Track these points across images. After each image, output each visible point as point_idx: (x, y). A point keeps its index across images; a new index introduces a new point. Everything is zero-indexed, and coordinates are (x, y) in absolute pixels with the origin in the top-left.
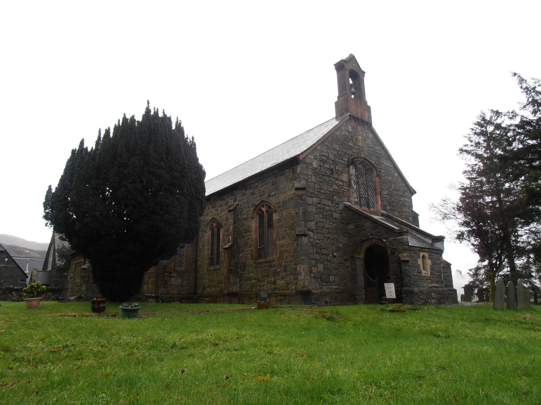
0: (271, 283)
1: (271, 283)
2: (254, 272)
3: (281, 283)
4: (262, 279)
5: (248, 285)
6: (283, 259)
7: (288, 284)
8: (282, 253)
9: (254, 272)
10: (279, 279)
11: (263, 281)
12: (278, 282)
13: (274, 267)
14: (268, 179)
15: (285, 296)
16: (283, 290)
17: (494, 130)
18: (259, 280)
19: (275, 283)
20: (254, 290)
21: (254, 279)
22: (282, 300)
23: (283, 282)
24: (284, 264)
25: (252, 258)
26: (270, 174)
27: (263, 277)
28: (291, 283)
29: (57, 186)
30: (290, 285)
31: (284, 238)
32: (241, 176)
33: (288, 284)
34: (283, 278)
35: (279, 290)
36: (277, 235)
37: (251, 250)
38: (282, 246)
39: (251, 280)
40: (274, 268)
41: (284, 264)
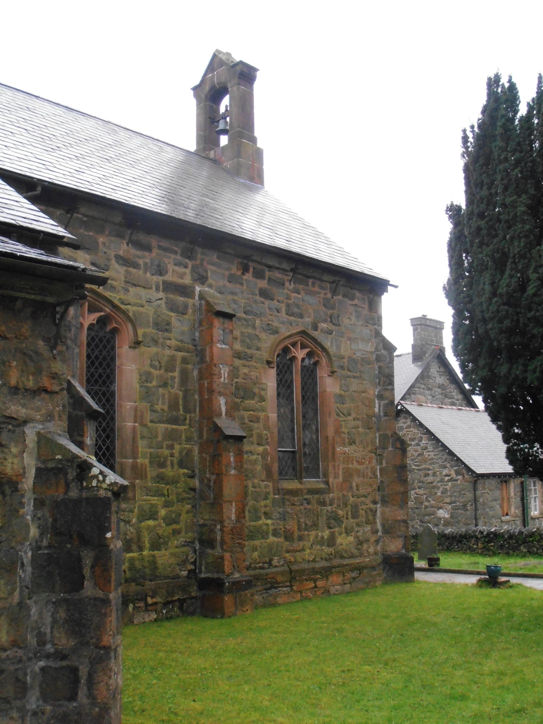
0: (321, 542)
1: (321, 542)
2: (276, 515)
3: (345, 541)
4: (296, 534)
5: (255, 549)
6: (351, 488)
7: (361, 543)
8: (348, 475)
9: (276, 515)
10: (340, 534)
11: (301, 538)
12: (339, 540)
13: (331, 505)
14: (313, 284)
15: (360, 569)
16: (352, 556)
17: (510, 369)
18: (288, 537)
19: (331, 542)
20: (275, 562)
21: (275, 533)
22: (354, 579)
23: (351, 539)
24: (352, 499)
25: (269, 475)
26: (326, 277)
27: (299, 529)
28: (367, 541)
29: (480, 116)
30: (365, 546)
31: (352, 442)
32: (118, 181)
33: (361, 543)
34: (348, 532)
35: (342, 557)
36: (338, 432)
37: (264, 455)
38: (348, 459)
39: (265, 535)
40: (329, 508)
41: (352, 499)
